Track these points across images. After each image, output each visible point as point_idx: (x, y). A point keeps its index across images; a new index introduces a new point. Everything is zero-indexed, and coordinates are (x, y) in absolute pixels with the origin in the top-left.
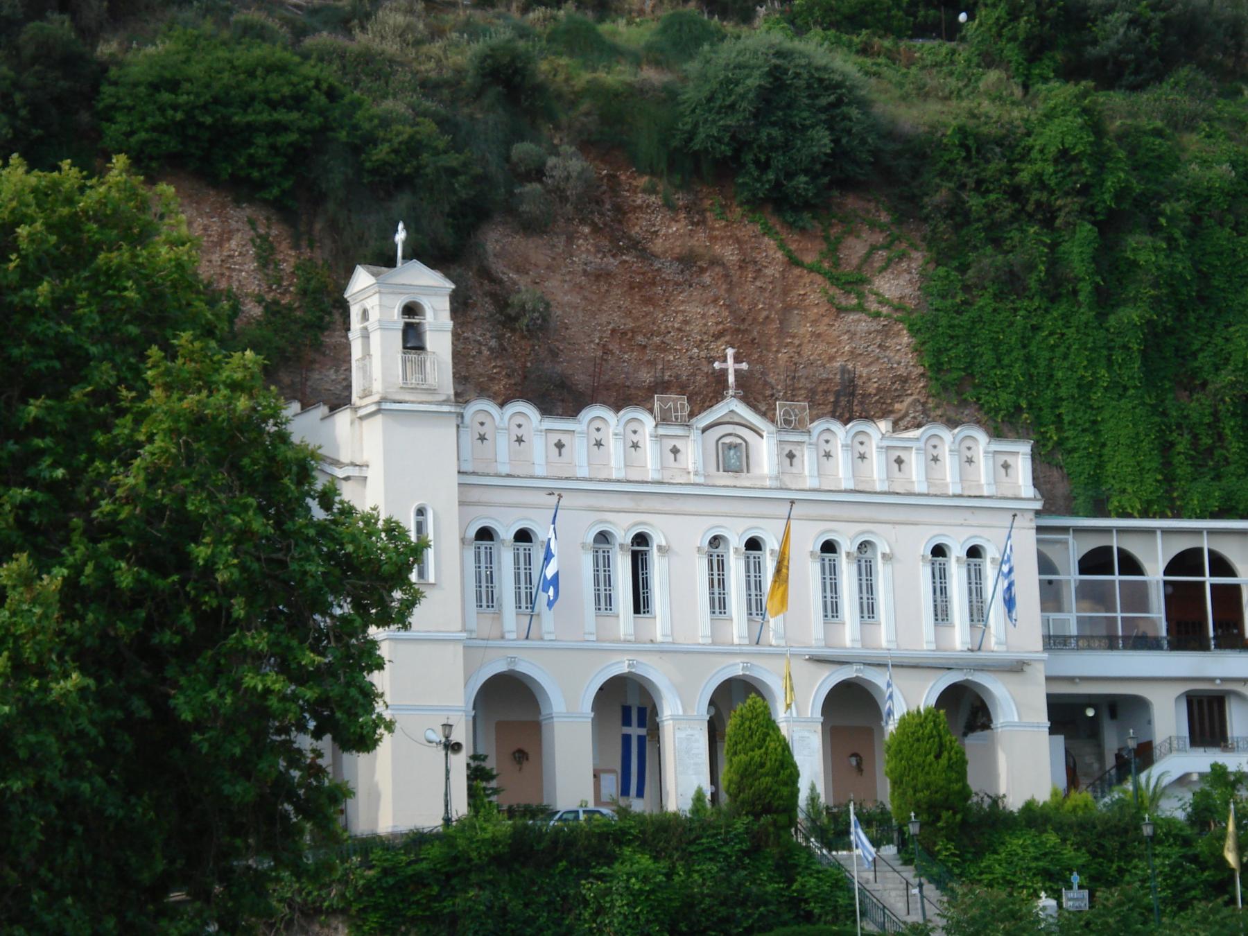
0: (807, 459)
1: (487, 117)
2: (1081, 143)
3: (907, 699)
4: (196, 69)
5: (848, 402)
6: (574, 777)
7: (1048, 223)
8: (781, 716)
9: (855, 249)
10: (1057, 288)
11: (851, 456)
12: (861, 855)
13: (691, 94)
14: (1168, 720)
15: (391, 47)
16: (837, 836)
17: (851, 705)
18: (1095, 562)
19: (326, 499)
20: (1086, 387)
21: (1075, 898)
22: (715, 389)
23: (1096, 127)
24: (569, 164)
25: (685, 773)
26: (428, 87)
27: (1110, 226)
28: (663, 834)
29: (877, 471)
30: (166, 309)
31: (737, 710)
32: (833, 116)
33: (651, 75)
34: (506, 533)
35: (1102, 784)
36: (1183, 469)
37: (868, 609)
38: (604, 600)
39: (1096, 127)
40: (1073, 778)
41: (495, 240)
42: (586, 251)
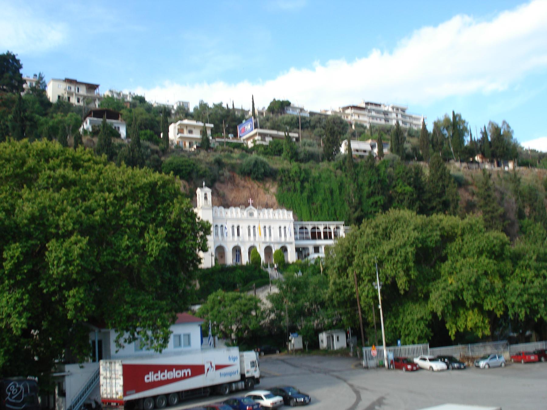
0: (261, 214)
1: (216, 167)
2: (298, 170)
3: (275, 248)
4: (175, 161)
5: (267, 206)
6: (230, 260)
7: (294, 181)
8: (258, 250)
9: (268, 185)
10: (295, 190)
11: (268, 214)
12: (269, 270)
13: (244, 164)
14: (311, 250)
15: (202, 158)
16: (267, 267)
17: (268, 250)
18: (302, 228)
19: (199, 219)
20: (299, 205)
21: (300, 274)
22: (249, 204)
23: (300, 168)
24: (227, 174)
25: (245, 259)
26: (207, 163)
27: (302, 182)
28: (242, 267)
29: (271, 216)
30: (176, 194)
31: (252, 250)
32: (264, 167)
33: (239, 161)
34: (219, 225)
35: (302, 259)
36: (313, 215)
37: (270, 235)
38: (233, 234)
39: (300, 168)
40: (298, 258)
41: (217, 185)
42: (230, 186)
